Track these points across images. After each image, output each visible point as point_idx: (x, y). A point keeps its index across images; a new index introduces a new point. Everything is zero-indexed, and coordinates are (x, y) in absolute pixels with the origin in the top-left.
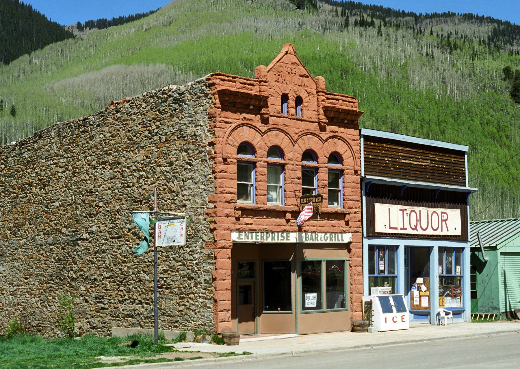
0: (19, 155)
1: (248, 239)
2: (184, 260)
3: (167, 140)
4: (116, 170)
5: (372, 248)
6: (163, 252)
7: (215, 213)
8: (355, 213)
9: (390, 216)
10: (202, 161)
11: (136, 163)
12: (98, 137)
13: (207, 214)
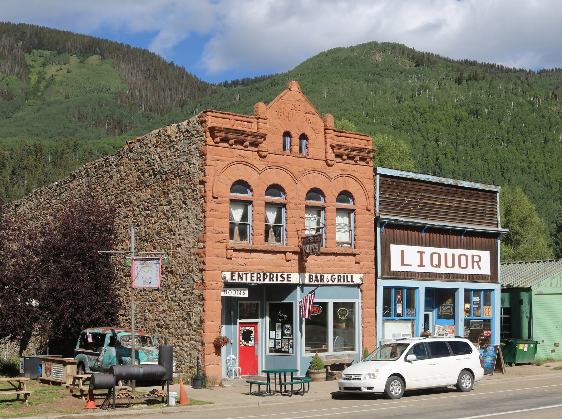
0: (59, 194)
1: (242, 279)
2: (180, 300)
3: (167, 179)
4: (129, 209)
5: (387, 290)
6: (163, 292)
7: (204, 253)
8: (367, 253)
9: (407, 257)
10: (194, 200)
11: (143, 202)
12: (116, 176)
13: (198, 254)
